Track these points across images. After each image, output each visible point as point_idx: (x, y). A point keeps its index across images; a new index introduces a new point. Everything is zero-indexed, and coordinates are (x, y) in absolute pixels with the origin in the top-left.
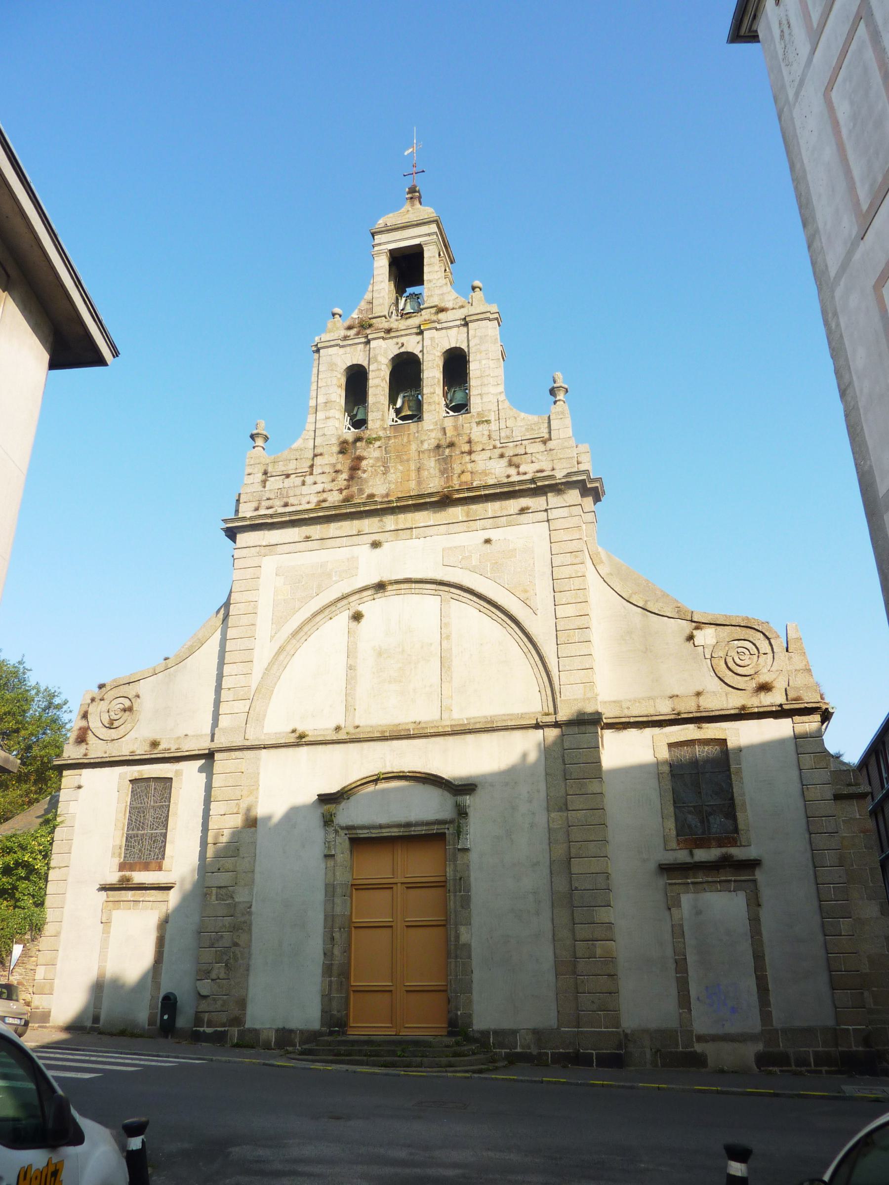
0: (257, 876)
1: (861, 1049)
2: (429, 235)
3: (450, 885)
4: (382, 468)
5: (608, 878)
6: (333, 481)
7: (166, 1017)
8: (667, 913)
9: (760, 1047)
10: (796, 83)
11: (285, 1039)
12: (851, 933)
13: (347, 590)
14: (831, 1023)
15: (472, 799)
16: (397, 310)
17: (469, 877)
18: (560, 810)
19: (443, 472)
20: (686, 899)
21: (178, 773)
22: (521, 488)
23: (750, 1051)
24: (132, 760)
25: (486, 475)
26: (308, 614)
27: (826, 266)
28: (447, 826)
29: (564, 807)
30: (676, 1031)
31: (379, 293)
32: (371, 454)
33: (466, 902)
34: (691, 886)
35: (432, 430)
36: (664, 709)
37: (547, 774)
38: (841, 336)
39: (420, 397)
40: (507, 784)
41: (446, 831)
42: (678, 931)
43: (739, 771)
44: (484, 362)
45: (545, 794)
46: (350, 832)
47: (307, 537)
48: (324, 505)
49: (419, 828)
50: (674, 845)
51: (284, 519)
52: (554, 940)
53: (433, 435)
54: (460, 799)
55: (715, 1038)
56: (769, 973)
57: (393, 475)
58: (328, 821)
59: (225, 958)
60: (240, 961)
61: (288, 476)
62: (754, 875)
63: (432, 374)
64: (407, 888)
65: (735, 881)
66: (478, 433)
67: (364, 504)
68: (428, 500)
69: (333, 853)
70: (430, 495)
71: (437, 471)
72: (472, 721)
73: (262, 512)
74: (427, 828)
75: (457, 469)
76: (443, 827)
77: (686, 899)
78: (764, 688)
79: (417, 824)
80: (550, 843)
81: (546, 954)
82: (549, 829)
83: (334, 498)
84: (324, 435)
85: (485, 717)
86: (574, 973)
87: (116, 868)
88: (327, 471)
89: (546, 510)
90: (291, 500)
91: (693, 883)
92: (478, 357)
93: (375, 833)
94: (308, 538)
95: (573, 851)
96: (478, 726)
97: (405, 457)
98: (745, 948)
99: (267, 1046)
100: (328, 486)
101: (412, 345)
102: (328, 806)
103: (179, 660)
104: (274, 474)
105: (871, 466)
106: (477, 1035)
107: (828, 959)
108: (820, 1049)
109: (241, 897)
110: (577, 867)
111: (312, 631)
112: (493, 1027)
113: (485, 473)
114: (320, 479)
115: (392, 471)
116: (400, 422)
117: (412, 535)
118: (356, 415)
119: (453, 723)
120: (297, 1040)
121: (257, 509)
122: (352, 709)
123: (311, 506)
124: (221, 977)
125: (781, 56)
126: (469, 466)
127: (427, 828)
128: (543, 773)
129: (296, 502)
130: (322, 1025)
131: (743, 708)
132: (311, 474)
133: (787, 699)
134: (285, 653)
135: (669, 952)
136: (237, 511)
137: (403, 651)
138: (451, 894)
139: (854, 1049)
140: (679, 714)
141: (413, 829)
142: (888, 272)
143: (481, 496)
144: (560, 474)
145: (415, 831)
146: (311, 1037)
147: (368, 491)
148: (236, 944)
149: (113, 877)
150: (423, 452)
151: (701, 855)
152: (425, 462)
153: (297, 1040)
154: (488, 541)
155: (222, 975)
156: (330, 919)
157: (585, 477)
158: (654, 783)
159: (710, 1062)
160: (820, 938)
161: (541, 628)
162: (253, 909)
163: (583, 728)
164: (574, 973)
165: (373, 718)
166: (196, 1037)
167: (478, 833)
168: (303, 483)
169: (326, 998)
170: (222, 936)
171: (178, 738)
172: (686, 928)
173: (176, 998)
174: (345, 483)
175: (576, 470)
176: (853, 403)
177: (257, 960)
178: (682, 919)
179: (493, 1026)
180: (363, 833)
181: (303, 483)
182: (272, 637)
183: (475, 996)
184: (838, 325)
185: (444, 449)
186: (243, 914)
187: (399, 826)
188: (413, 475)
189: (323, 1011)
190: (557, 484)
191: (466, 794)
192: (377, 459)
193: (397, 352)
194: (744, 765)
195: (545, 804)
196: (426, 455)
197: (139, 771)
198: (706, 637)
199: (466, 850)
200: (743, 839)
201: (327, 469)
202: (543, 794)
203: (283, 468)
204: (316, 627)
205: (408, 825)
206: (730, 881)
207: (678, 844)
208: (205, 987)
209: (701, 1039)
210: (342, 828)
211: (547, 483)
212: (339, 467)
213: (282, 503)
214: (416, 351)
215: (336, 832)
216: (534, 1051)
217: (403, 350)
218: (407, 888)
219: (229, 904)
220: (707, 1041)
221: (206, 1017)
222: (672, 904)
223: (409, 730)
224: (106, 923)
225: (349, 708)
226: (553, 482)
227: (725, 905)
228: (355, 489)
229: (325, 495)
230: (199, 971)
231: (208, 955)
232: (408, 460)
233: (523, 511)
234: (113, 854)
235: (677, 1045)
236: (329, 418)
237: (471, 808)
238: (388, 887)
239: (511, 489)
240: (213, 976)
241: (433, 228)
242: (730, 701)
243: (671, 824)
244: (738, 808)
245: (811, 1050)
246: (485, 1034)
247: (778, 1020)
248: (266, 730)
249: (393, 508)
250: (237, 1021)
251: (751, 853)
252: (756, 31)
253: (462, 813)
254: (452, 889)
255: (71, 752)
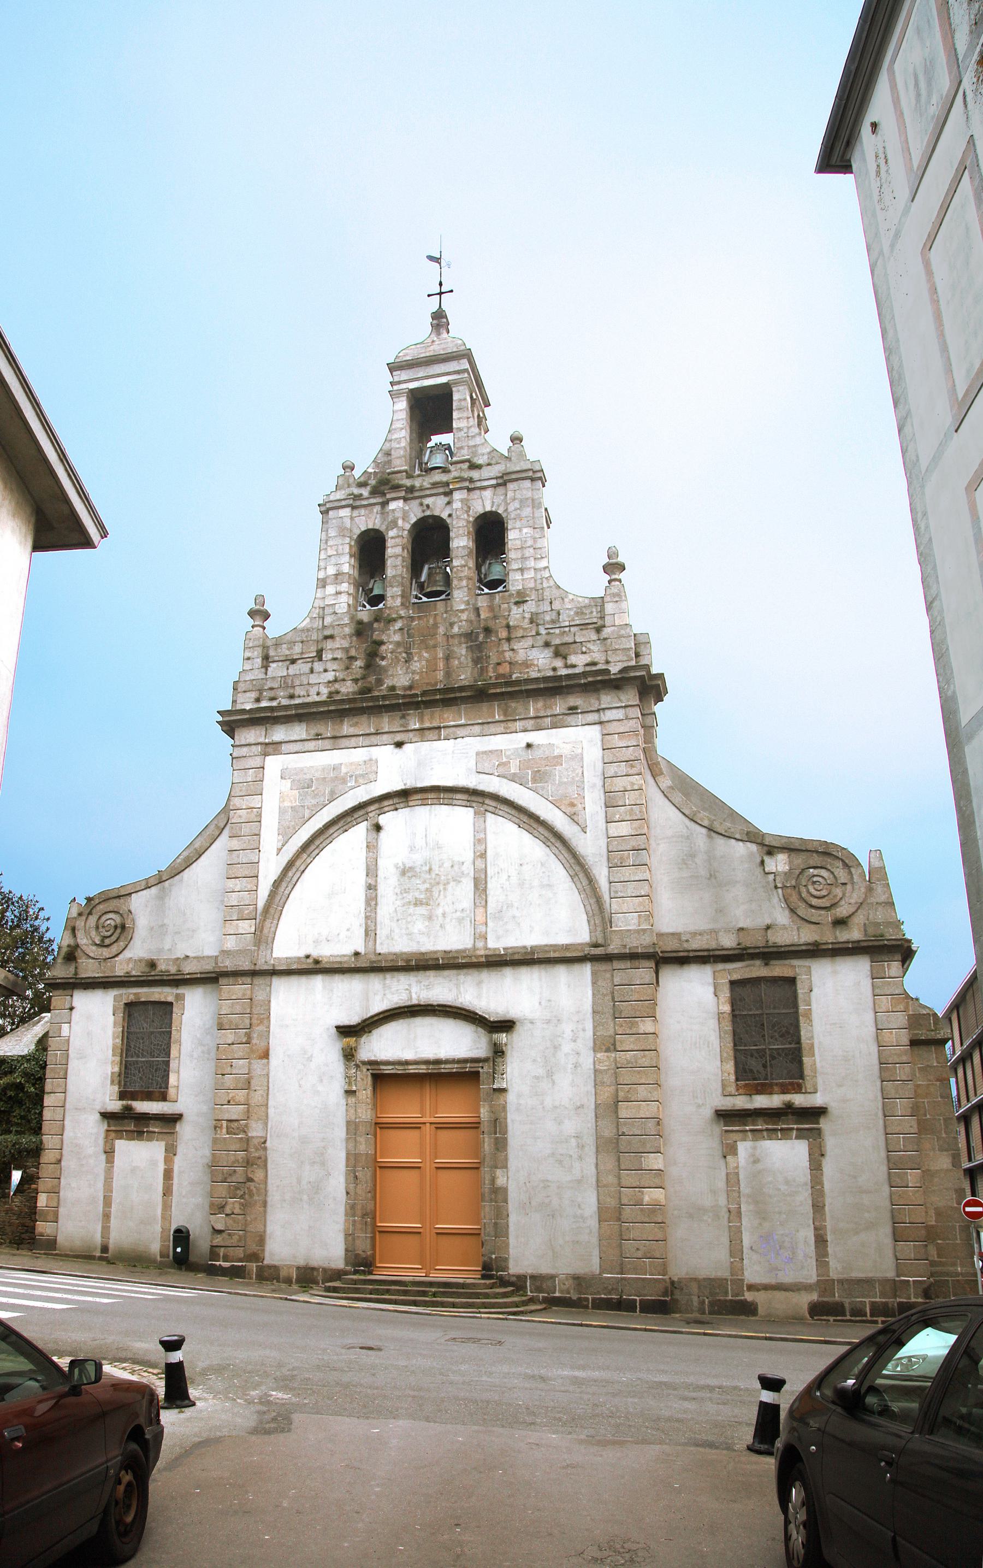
0: (271, 1111)
1: (920, 1300)
2: (458, 372)
3: (485, 1127)
4: (404, 655)
5: (658, 1124)
6: (347, 668)
7: (179, 1250)
8: (722, 1162)
9: (814, 1297)
10: (892, 233)
11: (307, 1277)
12: (918, 1185)
13: (365, 798)
14: (891, 1274)
15: (509, 1037)
16: (421, 464)
17: (506, 1119)
18: (608, 1050)
19: (476, 661)
20: (744, 1148)
21: (180, 998)
22: (568, 683)
23: (804, 1300)
24: (127, 982)
25: (528, 666)
26: (320, 825)
27: (917, 456)
28: (481, 1065)
29: (612, 1047)
30: (726, 1280)
31: (399, 443)
32: (392, 637)
33: (501, 1144)
34: (749, 1133)
35: (462, 611)
36: (728, 941)
37: (594, 1012)
38: (930, 539)
39: (448, 569)
40: (548, 1022)
41: (480, 1070)
42: (732, 1180)
43: (808, 1014)
44: (525, 530)
45: (591, 1033)
46: (373, 1067)
47: (318, 735)
48: (338, 697)
49: (447, 1066)
50: (732, 1089)
51: (289, 713)
52: (598, 1186)
53: (464, 616)
54: (495, 1036)
55: (766, 1287)
56: (829, 1224)
57: (418, 664)
58: (349, 1055)
59: (240, 1193)
60: (256, 1198)
61: (293, 662)
62: (818, 1123)
63: (461, 542)
64: (437, 1128)
65: (797, 1129)
66: (516, 615)
67: (384, 697)
68: (458, 695)
69: (354, 1088)
70: (462, 689)
71: (470, 660)
72: (510, 951)
73: (264, 704)
74: (459, 1066)
75: (494, 659)
76: (476, 1065)
77: (744, 1148)
78: (840, 923)
79: (447, 1062)
80: (596, 1085)
81: (589, 1202)
82: (596, 1071)
83: (348, 688)
84: (335, 613)
85: (525, 947)
86: (619, 1219)
87: (116, 1096)
88: (339, 657)
89: (598, 711)
90: (299, 691)
91: (751, 1131)
92: (518, 524)
93: (399, 1070)
94: (318, 737)
95: (621, 1094)
96: (516, 957)
97: (431, 643)
98: (804, 1198)
99: (288, 1281)
100: (340, 675)
101: (438, 506)
102: (348, 1039)
103: (175, 872)
104: (277, 658)
105: (954, 692)
106: (514, 1279)
107: (892, 1211)
108: (878, 1300)
109: (255, 1131)
110: (625, 1111)
111: (324, 844)
112: (530, 1271)
113: (527, 664)
114: (331, 666)
115: (416, 659)
116: (425, 599)
117: (440, 735)
118: (371, 590)
119: (488, 952)
120: (320, 1278)
121: (258, 700)
122: (373, 934)
123: (323, 698)
124: (236, 1212)
125: (876, 198)
126: (508, 655)
127: (459, 1066)
128: (590, 1010)
129: (302, 694)
130: (347, 1264)
131: (816, 944)
132: (320, 659)
133: (866, 935)
134: (294, 869)
135: (722, 1201)
136: (234, 702)
137: (430, 870)
138: (487, 1138)
139: (913, 1300)
140: (745, 949)
141: (443, 1066)
142: (982, 476)
143: (521, 691)
144: (614, 669)
145: (444, 1068)
146: (337, 1275)
147: (388, 682)
148: (250, 1180)
149: (115, 1106)
150: (452, 637)
151: (761, 1101)
152: (455, 649)
153: (320, 1278)
154: (529, 746)
155: (237, 1211)
156: (353, 1160)
157: (644, 673)
158: (713, 1023)
159: (761, 1311)
160: (886, 1189)
161: (591, 845)
162: (268, 1144)
163: (636, 963)
164: (619, 1219)
165: (397, 940)
166: (212, 1271)
167: (517, 1074)
168: (312, 671)
169: (350, 1237)
170: (235, 1171)
171: (178, 959)
172: (741, 1177)
173: (188, 1232)
174: (360, 671)
175: (633, 663)
176: (938, 619)
177: (274, 1196)
178: (737, 1167)
179: (530, 1271)
180: (388, 1070)
181: (312, 671)
182: (279, 850)
183: (512, 1240)
184: (927, 527)
185: (480, 638)
186: (257, 1149)
187: (427, 1062)
188: (441, 665)
189: (346, 1250)
190: (611, 680)
191: (502, 1032)
192: (398, 644)
193: (420, 515)
194: (814, 1006)
195: (591, 1044)
196: (456, 641)
197: (135, 994)
198: (779, 863)
199: (503, 1091)
200: (809, 1085)
201: (339, 655)
202: (590, 1033)
203: (288, 652)
204: (330, 839)
205: (438, 1062)
206: (792, 1129)
207: (738, 1090)
208: (220, 1222)
209: (751, 1287)
210: (364, 1063)
211: (599, 678)
212: (353, 653)
213: (287, 694)
214: (444, 516)
215: (357, 1066)
216: (575, 1297)
217: (428, 513)
218: (437, 1128)
219: (241, 1138)
220: (758, 1290)
221: (222, 1252)
222: (729, 1150)
223: (438, 959)
224: (109, 1153)
225: (370, 933)
226: (606, 678)
227: (786, 1155)
228: (372, 679)
229: (337, 686)
230: (212, 1205)
231: (222, 1189)
232: (435, 646)
233: (573, 710)
234: (112, 1082)
235: (726, 1293)
236: (340, 593)
237: (509, 1047)
238: (416, 1126)
239: (557, 684)
240: (228, 1211)
241: (465, 364)
242: (802, 935)
243: (730, 1066)
244: (805, 1052)
245: (867, 1300)
246: (522, 1278)
247: (836, 1269)
248: (276, 954)
249: (418, 702)
250: (255, 1257)
251: (817, 1100)
252: (849, 161)
253: (498, 1052)
254: (486, 1131)
255: (60, 972)
